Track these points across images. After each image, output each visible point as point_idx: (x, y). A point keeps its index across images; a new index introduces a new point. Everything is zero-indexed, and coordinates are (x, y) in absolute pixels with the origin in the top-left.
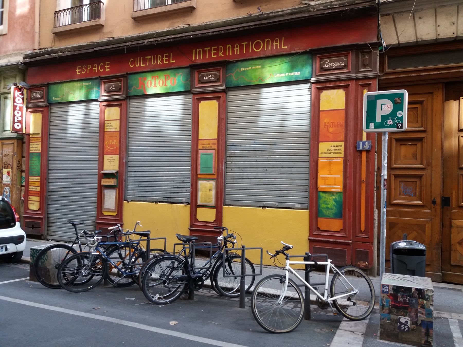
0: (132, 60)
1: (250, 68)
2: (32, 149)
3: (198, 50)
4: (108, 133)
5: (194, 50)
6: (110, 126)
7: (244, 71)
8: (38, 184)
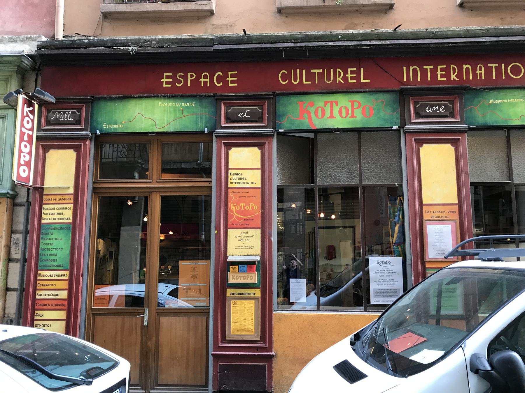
0: (219, 75)
1: (505, 101)
2: (49, 216)
3: (411, 68)
4: (235, 190)
5: (405, 68)
6: (241, 179)
7: (495, 105)
8: (65, 285)
